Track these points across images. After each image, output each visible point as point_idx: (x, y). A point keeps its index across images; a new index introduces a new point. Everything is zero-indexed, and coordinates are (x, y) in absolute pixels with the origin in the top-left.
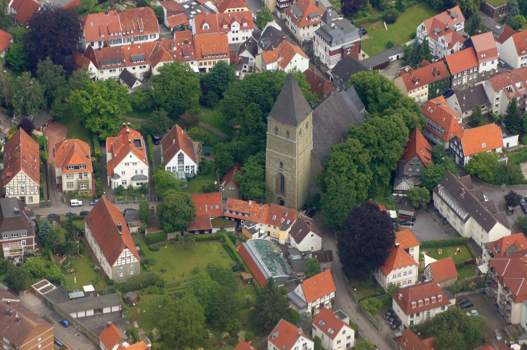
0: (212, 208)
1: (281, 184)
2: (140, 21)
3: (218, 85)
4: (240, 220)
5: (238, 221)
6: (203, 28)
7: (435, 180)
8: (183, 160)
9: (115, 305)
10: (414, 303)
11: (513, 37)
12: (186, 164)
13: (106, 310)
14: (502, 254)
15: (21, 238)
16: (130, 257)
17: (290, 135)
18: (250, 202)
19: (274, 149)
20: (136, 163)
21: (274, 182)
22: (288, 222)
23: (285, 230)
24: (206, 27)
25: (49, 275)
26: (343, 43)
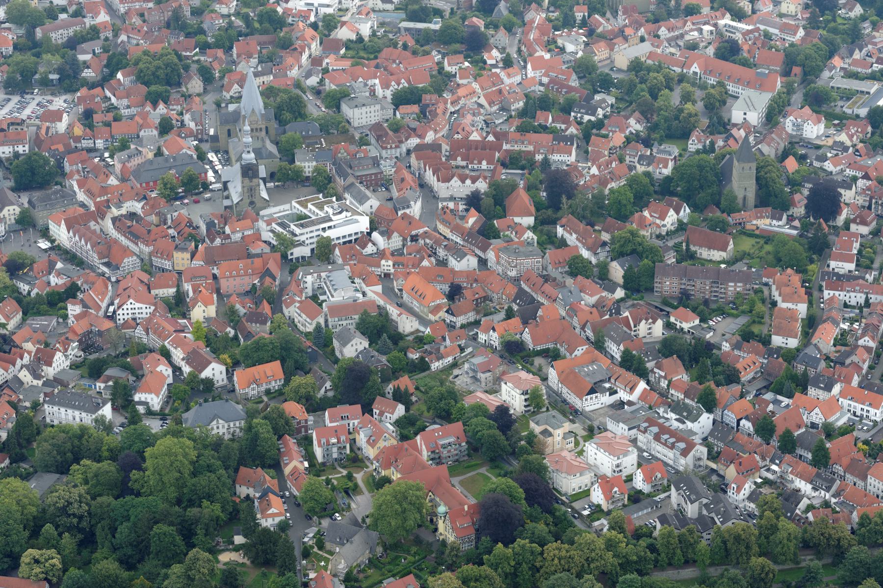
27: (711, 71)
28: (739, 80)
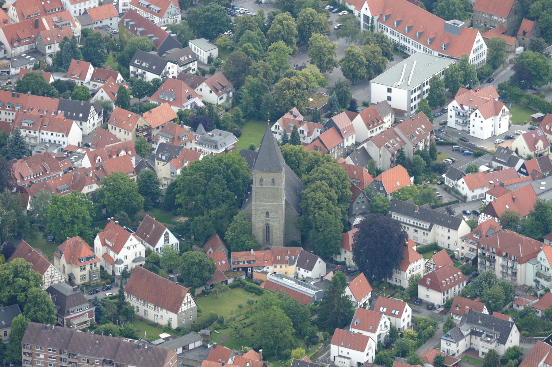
0: (220, 264)
1: (267, 235)
2: (45, 164)
3: (151, 189)
4: (248, 268)
6: (97, 161)
8: (168, 240)
13: (191, 346)
15: (85, 312)
16: (190, 301)
17: (275, 182)
22: (293, 258)
23: (293, 264)
27: (388, 17)
28: (421, 34)
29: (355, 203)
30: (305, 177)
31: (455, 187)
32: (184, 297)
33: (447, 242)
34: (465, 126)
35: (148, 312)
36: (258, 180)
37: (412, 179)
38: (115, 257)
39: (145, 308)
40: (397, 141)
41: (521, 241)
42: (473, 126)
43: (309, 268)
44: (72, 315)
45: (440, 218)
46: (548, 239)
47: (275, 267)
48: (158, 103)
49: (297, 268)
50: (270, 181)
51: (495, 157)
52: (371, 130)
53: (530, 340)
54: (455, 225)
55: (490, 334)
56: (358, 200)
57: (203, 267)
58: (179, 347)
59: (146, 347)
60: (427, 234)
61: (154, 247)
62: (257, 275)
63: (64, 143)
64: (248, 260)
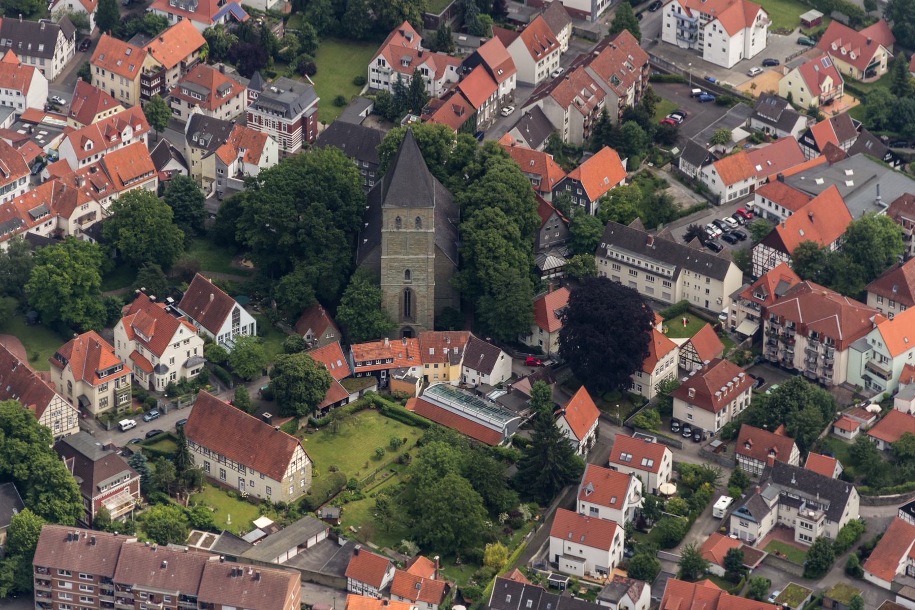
5: (376, 374)
6: (86, 148)
7: (595, 239)
8: (239, 320)
9: (320, 532)
10: (718, 393)
11: (524, 39)
12: (242, 324)
13: (311, 543)
14: (773, 297)
15: (124, 484)
17: (423, 223)
18: (387, 341)
19: (396, 253)
20: (188, 341)
21: (396, 304)
22: (456, 350)
23: (458, 363)
24: (89, 146)
25: (201, 520)
26: (302, 109)
29: (543, 231)
30: (462, 195)
31: (699, 177)
32: (292, 453)
33: (703, 297)
34: (694, 43)
35: (227, 473)
36: (393, 220)
37: (624, 163)
38: (153, 360)
39: (221, 465)
40: (592, 92)
41: (836, 308)
42: (710, 45)
43: (486, 369)
44: (105, 492)
45: (692, 259)
46: (874, 292)
47: (427, 367)
48: (167, 15)
49: (465, 368)
50: (413, 221)
51: (756, 112)
52: (541, 61)
53: (873, 500)
54: (719, 274)
55: (812, 503)
56: (548, 225)
57: (313, 383)
58: (292, 547)
59: (251, 572)
60: (670, 285)
61: (215, 334)
62: (397, 386)
63: (20, 105)
64: (380, 358)
